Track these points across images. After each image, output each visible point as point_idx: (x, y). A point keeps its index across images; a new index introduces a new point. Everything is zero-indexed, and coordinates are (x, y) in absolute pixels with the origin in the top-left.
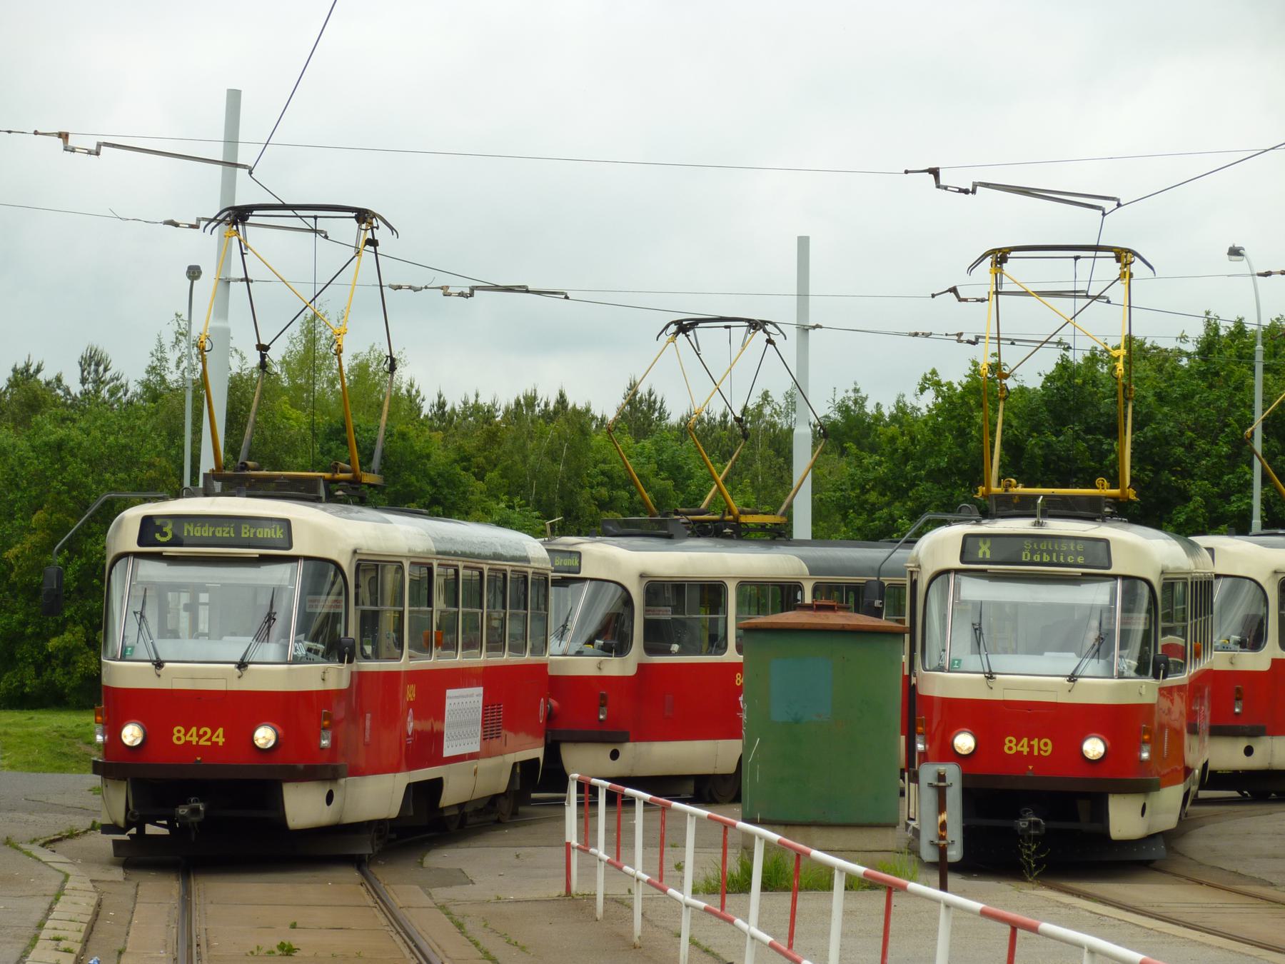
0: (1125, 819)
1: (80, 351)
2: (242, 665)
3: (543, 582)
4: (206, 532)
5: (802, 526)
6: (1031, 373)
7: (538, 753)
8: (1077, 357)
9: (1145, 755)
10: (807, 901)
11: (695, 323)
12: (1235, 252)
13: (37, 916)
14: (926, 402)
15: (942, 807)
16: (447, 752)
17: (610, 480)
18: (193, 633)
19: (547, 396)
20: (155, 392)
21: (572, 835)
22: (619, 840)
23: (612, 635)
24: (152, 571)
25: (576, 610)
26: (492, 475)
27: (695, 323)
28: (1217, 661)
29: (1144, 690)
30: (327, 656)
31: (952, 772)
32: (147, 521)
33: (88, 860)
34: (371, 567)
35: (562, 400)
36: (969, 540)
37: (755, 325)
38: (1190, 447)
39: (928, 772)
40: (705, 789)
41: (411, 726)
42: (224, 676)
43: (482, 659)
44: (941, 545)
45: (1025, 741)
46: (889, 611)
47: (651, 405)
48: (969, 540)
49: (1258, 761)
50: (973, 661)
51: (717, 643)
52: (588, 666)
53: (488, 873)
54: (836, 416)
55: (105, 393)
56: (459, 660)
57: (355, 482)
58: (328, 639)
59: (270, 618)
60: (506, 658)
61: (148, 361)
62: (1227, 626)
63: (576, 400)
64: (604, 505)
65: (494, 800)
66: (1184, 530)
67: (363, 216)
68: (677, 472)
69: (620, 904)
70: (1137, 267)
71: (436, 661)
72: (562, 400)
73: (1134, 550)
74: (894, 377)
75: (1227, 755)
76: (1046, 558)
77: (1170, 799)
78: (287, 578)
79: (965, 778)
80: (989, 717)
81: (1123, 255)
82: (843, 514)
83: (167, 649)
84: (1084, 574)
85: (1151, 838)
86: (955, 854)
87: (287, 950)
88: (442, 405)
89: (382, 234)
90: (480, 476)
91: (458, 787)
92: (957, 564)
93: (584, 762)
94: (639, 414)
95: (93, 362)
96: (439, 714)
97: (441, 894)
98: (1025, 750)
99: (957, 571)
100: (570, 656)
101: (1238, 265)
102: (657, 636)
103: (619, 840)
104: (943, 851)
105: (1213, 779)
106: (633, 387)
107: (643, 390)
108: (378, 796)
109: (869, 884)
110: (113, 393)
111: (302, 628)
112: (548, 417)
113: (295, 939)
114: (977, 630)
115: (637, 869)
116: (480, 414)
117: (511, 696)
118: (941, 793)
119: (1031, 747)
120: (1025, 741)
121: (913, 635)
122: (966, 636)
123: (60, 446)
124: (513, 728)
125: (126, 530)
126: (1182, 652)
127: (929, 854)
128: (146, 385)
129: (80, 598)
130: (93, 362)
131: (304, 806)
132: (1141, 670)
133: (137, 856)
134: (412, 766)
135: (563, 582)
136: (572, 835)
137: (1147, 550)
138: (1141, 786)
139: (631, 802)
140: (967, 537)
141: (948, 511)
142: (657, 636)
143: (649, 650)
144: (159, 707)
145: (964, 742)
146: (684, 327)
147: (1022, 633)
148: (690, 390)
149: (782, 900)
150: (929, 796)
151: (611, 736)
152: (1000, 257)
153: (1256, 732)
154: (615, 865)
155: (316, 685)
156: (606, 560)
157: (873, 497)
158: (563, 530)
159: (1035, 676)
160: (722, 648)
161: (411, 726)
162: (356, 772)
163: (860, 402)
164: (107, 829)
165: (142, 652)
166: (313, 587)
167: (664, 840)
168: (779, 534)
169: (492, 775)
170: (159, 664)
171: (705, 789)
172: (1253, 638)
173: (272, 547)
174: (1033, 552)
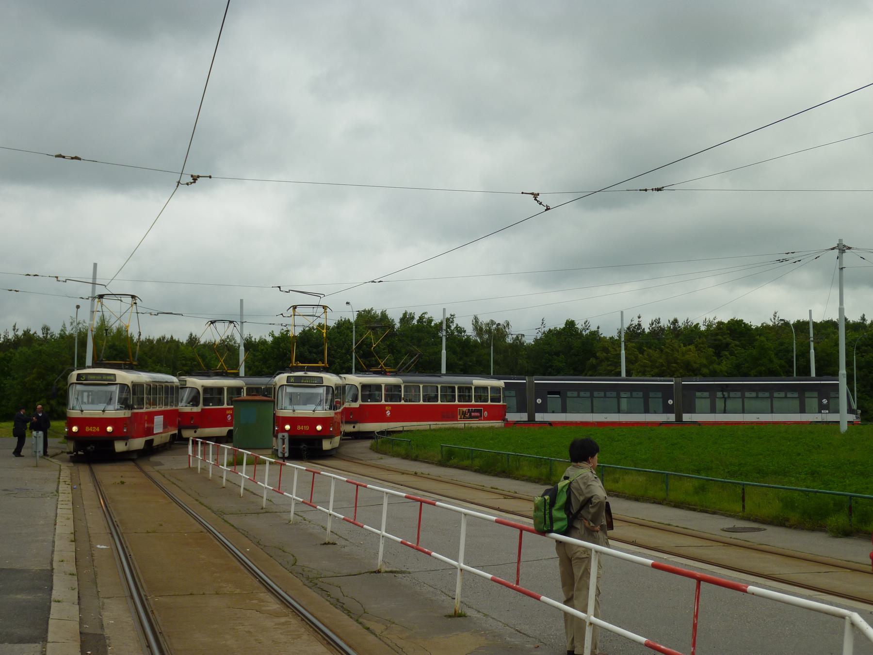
0: (326, 445)
1: (41, 326)
2: (104, 411)
3: (177, 387)
4: (94, 377)
5: (242, 373)
6: (297, 331)
7: (176, 432)
10: (258, 467)
11: (215, 321)
12: (348, 303)
13: (57, 476)
14: (269, 339)
15: (284, 444)
16: (155, 432)
18: (87, 404)
19: (168, 336)
20: (62, 336)
21: (190, 453)
22: (205, 454)
23: (194, 401)
24: (79, 387)
25: (186, 395)
27: (215, 321)
28: (347, 405)
29: (331, 413)
30: (125, 409)
31: (286, 435)
32: (79, 375)
33: (63, 460)
34: (137, 386)
37: (231, 322)
38: (335, 351)
39: (280, 435)
40: (218, 440)
41: (146, 425)
42: (99, 414)
43: (164, 408)
44: (281, 378)
46: (269, 395)
49: (356, 430)
50: (290, 407)
51: (221, 402)
52: (188, 409)
53: (168, 462)
55: (49, 336)
56: (157, 409)
57: (131, 364)
58: (125, 404)
59: (111, 399)
60: (169, 408)
61: (61, 328)
62: (349, 396)
63: (176, 338)
65: (165, 444)
66: (337, 373)
67: (133, 297)
68: (203, 357)
69: (205, 470)
70: (328, 310)
71: (151, 409)
73: (329, 379)
74: (262, 331)
75: (349, 428)
77: (337, 440)
78: (115, 389)
80: (294, 421)
81: (325, 307)
82: (253, 371)
83: (84, 407)
85: (332, 449)
86: (287, 455)
87: (122, 483)
89: (138, 301)
91: (157, 441)
93: (187, 433)
94: (193, 341)
95: (46, 329)
96: (153, 423)
97: (157, 468)
100: (184, 407)
101: (349, 306)
102: (206, 402)
103: (205, 454)
104: (284, 454)
105: (347, 434)
107: (194, 335)
108: (138, 443)
109: (275, 463)
111: (119, 402)
112: (167, 341)
113: (123, 480)
114: (291, 399)
117: (171, 418)
118: (283, 440)
121: (274, 402)
122: (288, 401)
123: (40, 351)
124: (171, 426)
125: (73, 376)
126: (340, 403)
127: (280, 455)
128: (60, 334)
130: (46, 329)
131: (120, 447)
132: (330, 409)
133: (76, 460)
134: (146, 436)
135: (182, 388)
136: (190, 453)
137: (331, 379)
138: (330, 437)
139: (264, 462)
141: (283, 370)
142: (206, 402)
143: (204, 405)
144: (82, 422)
146: (212, 322)
147: (303, 399)
148: (209, 335)
149: (252, 467)
150: (280, 441)
151: (195, 427)
152: (295, 307)
153: (356, 422)
154: (204, 460)
155: (122, 416)
156: (193, 383)
157: (257, 363)
158: (180, 375)
159: (93, 411)
160: (223, 404)
161: (146, 425)
162: (133, 437)
163: (250, 338)
164: (68, 453)
165: (77, 408)
166: (121, 391)
167: (218, 453)
168: (236, 376)
169: (166, 437)
170: (82, 411)
171: (228, 438)
172: (355, 400)
173: (110, 380)
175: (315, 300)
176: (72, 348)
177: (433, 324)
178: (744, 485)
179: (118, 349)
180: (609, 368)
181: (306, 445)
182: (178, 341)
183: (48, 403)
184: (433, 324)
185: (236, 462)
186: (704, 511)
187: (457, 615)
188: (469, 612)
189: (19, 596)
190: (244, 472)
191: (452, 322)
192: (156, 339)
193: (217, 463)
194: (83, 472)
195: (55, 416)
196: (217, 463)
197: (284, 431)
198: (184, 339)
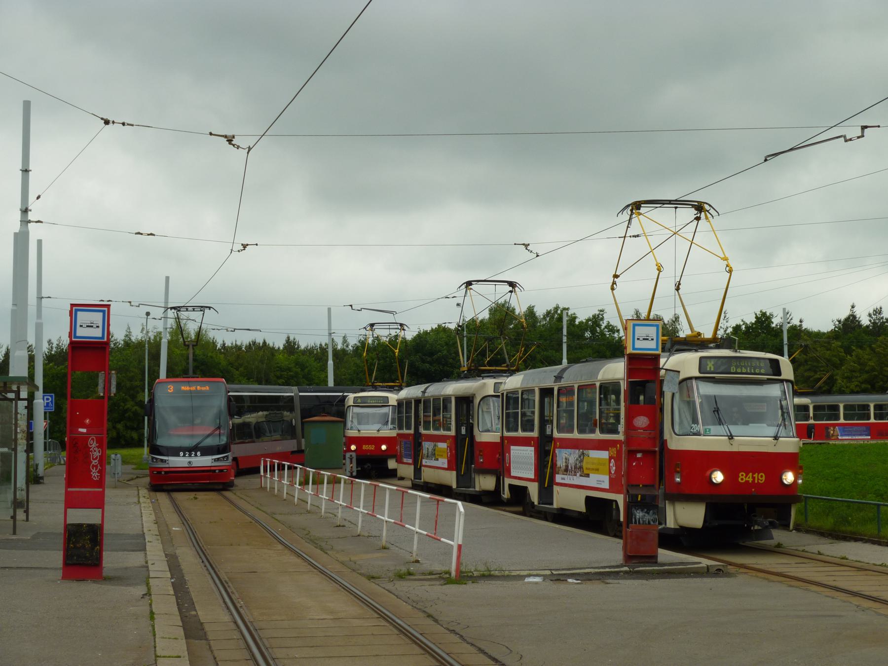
8: (519, 305)
9: (678, 480)
17: (281, 369)
20: (128, 344)
26: (241, 369)
31: (354, 454)
35: (265, 342)
36: (703, 360)
39: (348, 455)
45: (751, 475)
47: (295, 343)
48: (703, 360)
54: (359, 344)
61: (125, 333)
63: (270, 342)
64: (278, 378)
68: (303, 366)
69: (272, 488)
72: (265, 342)
76: (744, 370)
79: (357, 456)
83: (360, 427)
84: (768, 379)
86: (354, 474)
88: (224, 344)
90: (237, 370)
92: (697, 374)
98: (751, 480)
99: (697, 378)
106: (288, 338)
107: (291, 338)
110: (115, 344)
115: (285, 482)
116: (238, 348)
118: (351, 459)
119: (754, 478)
120: (751, 475)
128: (124, 341)
129: (630, 372)
139: (296, 468)
140: (701, 358)
145: (353, 447)
149: (315, 486)
152: (372, 325)
159: (370, 430)
174: (737, 367)
175: (389, 318)
176: (141, 360)
177: (577, 323)
178: (879, 505)
179: (198, 358)
180: (806, 374)
181: (373, 465)
182: (273, 348)
183: (114, 427)
184: (577, 323)
185: (305, 483)
186: (856, 540)
187: (384, 548)
188: (346, 523)
189: (188, 388)
190: (310, 490)
191: (602, 319)
192: (244, 344)
193: (292, 484)
194: (162, 497)
195: (123, 442)
196: (292, 484)
197: (349, 450)
198: (279, 343)
